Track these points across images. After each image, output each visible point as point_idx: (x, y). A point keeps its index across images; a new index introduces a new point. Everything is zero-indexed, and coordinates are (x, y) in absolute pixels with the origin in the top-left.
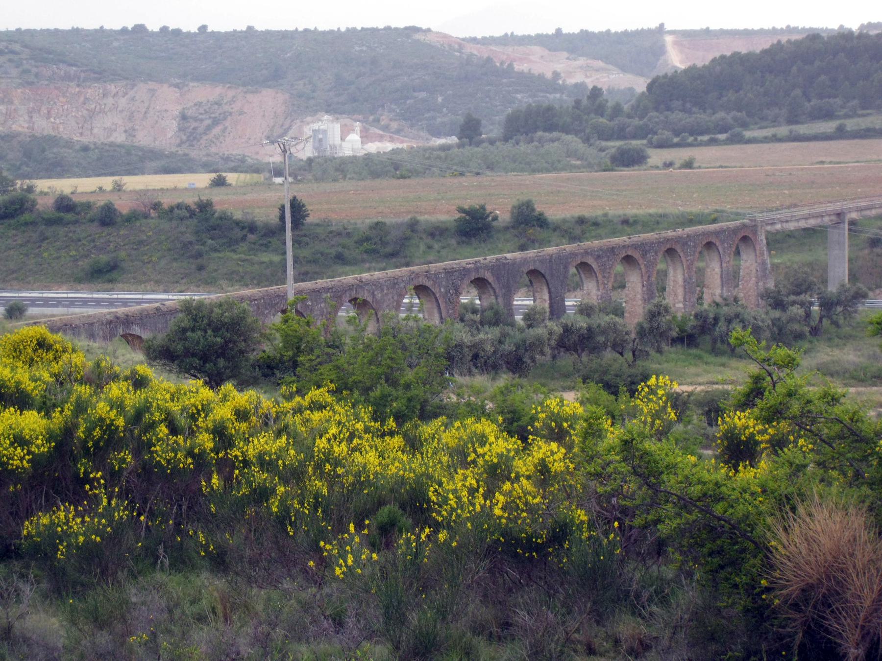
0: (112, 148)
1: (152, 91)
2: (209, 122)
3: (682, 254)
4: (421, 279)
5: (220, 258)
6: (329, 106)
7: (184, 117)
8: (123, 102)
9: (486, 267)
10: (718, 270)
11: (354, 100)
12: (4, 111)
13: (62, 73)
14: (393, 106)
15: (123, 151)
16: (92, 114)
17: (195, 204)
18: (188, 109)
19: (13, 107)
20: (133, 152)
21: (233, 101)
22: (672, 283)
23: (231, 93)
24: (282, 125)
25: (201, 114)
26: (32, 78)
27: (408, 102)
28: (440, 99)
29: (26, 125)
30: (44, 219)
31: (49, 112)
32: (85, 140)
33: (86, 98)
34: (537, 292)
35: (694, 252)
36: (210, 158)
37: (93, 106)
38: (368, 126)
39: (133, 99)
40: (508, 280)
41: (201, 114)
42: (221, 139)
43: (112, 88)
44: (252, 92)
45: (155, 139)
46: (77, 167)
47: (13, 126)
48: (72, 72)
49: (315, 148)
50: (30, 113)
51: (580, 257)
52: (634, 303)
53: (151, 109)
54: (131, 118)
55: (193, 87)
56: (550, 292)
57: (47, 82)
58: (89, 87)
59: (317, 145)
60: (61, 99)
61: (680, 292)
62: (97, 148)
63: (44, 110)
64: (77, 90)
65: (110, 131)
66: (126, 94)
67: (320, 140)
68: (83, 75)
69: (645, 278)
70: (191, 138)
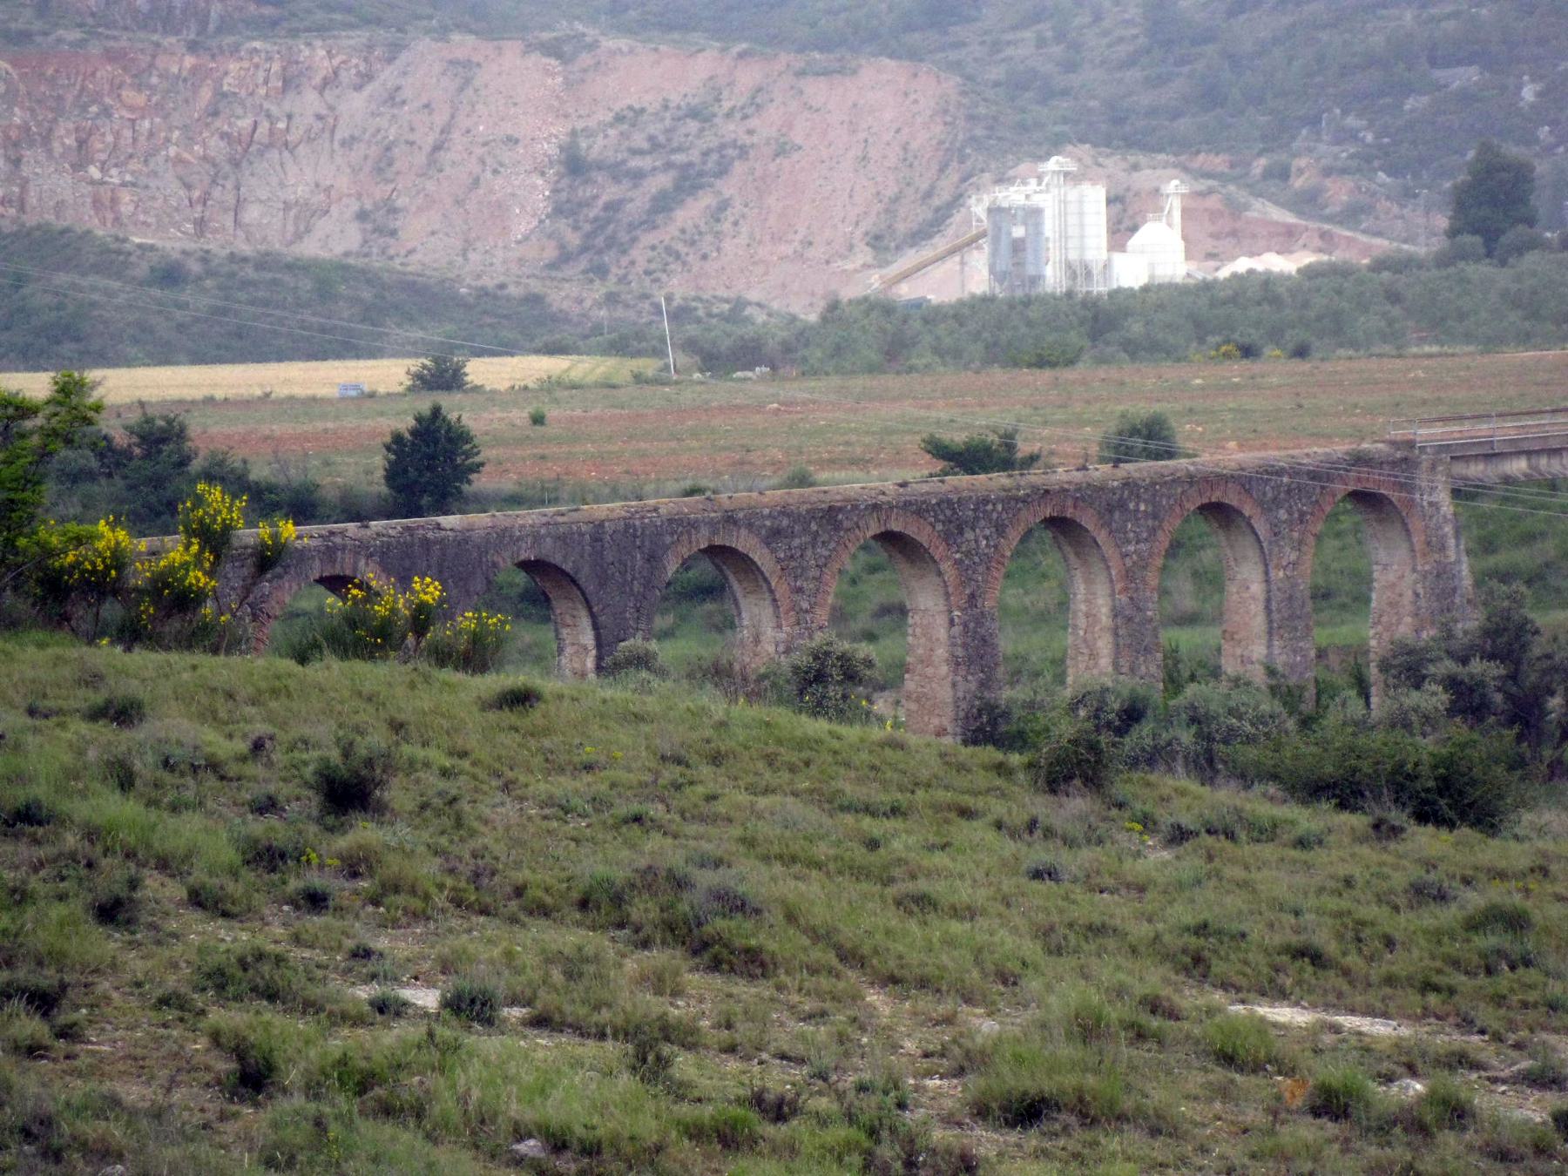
0: (269, 276)
1: (463, 70)
2: (664, 181)
3: (1102, 537)
6: (1118, 121)
7: (574, 165)
8: (355, 106)
10: (1257, 588)
11: (1211, 97)
14: (1351, 121)
15: (306, 284)
16: (243, 151)
18: (589, 133)
21: (756, 102)
23: (748, 76)
24: (929, 194)
25: (635, 152)
27: (1409, 104)
28: (1528, 93)
31: (81, 143)
33: (221, 95)
35: (1153, 531)
36: (620, 312)
37: (245, 123)
38: (1242, 196)
39: (393, 98)
41: (635, 152)
42: (707, 244)
43: (317, 56)
45: (467, 246)
46: (135, 341)
49: (997, 275)
51: (705, 531)
52: (930, 671)
53: (456, 135)
54: (383, 165)
55: (613, 53)
56: (596, 627)
57: (75, 35)
58: (234, 50)
59: (1004, 264)
60: (128, 95)
61: (1104, 645)
62: (210, 273)
64: (189, 61)
65: (305, 215)
66: (367, 77)
67: (1018, 247)
69: (959, 600)
70: (599, 241)
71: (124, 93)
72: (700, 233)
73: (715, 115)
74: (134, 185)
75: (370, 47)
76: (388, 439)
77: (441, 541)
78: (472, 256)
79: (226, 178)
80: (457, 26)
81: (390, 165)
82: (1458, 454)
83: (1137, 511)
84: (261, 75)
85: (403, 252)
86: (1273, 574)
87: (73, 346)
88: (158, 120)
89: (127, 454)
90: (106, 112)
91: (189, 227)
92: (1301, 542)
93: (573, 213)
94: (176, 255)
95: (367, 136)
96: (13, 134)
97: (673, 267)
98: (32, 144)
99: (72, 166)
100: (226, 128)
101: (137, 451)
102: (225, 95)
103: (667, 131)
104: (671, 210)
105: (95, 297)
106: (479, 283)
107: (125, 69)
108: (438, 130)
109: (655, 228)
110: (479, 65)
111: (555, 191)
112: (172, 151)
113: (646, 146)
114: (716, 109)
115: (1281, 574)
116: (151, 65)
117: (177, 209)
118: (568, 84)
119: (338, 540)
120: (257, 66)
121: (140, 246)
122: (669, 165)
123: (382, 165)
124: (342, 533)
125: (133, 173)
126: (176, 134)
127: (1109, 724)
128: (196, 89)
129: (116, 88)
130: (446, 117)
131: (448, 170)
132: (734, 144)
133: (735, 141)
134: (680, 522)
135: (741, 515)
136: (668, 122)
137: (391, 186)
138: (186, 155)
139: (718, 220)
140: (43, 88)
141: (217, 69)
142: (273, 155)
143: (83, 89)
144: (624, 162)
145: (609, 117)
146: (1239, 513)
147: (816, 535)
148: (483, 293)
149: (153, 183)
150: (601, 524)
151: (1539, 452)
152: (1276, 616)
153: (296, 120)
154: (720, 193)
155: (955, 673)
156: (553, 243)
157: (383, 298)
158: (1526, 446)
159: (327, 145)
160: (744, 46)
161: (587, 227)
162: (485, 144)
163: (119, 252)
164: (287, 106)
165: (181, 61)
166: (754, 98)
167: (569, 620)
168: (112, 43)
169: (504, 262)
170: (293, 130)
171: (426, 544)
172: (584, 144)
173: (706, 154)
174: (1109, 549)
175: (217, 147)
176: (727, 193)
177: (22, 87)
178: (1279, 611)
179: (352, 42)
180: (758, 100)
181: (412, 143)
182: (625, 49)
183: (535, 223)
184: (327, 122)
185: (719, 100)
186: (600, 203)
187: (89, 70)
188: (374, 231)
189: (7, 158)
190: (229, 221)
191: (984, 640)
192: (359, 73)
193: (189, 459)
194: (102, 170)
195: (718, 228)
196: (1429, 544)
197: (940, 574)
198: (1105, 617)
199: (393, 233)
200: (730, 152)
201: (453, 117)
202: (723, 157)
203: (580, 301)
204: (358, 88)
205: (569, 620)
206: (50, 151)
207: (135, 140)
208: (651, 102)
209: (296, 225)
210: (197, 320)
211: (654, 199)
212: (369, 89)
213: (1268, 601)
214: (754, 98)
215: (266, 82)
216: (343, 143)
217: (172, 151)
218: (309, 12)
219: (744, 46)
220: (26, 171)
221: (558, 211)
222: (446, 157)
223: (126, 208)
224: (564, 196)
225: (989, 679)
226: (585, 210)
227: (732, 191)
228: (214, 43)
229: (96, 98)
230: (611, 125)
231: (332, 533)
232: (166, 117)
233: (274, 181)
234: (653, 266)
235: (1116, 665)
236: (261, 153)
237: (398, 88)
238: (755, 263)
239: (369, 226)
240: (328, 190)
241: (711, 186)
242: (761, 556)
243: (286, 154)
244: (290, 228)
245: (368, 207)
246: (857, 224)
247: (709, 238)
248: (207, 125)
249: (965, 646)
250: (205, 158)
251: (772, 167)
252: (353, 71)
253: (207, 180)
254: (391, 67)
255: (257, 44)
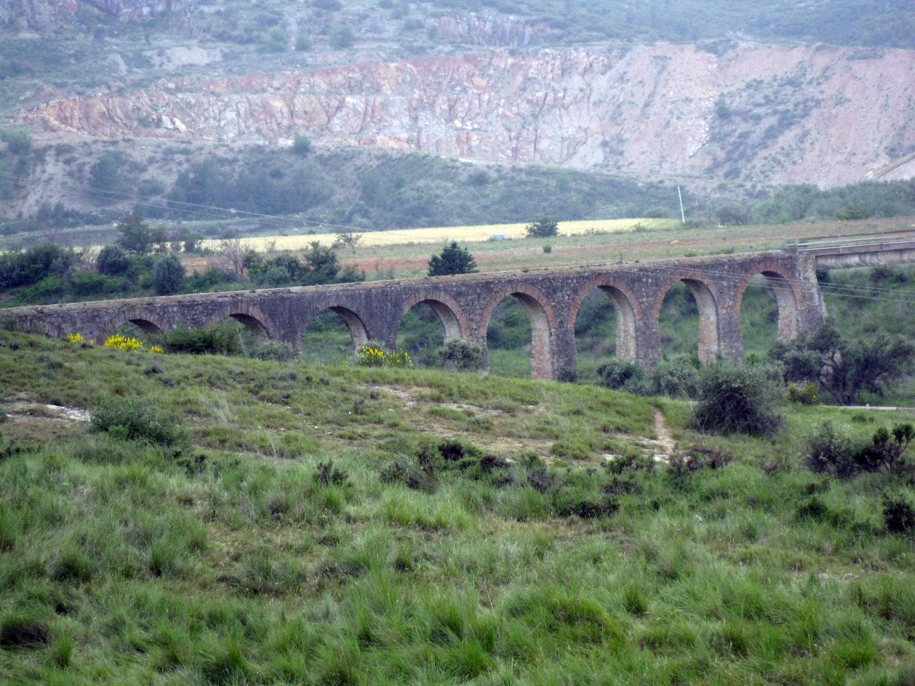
0: (533, 178)
1: (662, 62)
2: (773, 120)
3: (628, 294)
4: (137, 312)
5: (317, 340)
7: (723, 113)
8: (601, 83)
9: (251, 302)
10: (713, 318)
12: (361, 108)
13: (488, 27)
15: (553, 183)
16: (539, 109)
17: (308, 258)
18: (731, 95)
19: (379, 99)
20: (573, 185)
22: (622, 334)
23: (822, 60)
26: (421, 40)
29: (404, 135)
30: (73, 284)
31: (451, 108)
32: (479, 162)
33: (527, 79)
34: (356, 336)
35: (655, 293)
36: (727, 195)
37: (540, 94)
40: (290, 318)
42: (796, 156)
43: (580, 55)
44: (865, 58)
46: (460, 216)
47: (378, 138)
48: (508, 26)
50: (414, 112)
52: (542, 357)
53: (657, 98)
54: (616, 116)
57: (449, 48)
58: (535, 55)
60: (477, 80)
61: (632, 345)
63: (442, 104)
64: (511, 61)
65: (573, 145)
66: (609, 67)
68: (529, 30)
71: (474, 79)
72: (792, 150)
73: (802, 83)
74: (479, 130)
75: (610, 50)
76: (430, 260)
77: (290, 298)
78: (665, 165)
79: (530, 125)
80: (662, 37)
81: (620, 115)
82: (819, 255)
83: (647, 282)
84: (549, 68)
85: (627, 163)
86: (720, 311)
87: (426, 219)
88: (492, 94)
89: (306, 270)
90: (465, 90)
91: (509, 152)
92: (735, 296)
93: (722, 139)
94: (484, 169)
95: (607, 100)
96: (414, 104)
97: (776, 169)
98: (424, 109)
99: (446, 120)
100: (530, 97)
101: (312, 268)
102: (529, 79)
103: (776, 93)
104: (776, 137)
105: (438, 192)
106: (649, 180)
107: (476, 66)
108: (647, 95)
109: (768, 147)
110: (670, 59)
111: (712, 128)
112: (500, 110)
113: (763, 101)
114: (802, 79)
115: (724, 311)
116: (490, 64)
117: (502, 143)
118: (720, 68)
119: (239, 298)
120: (547, 63)
121: (464, 164)
122: (775, 112)
123: (616, 116)
124: (242, 295)
125: (478, 123)
126: (503, 101)
127: (614, 379)
128: (514, 76)
129: (470, 76)
130: (651, 88)
131: (652, 118)
132: (812, 99)
133: (813, 98)
134: (410, 289)
135: (441, 285)
136: (776, 88)
137: (620, 128)
138: (508, 113)
139: (802, 142)
140: (431, 78)
141: (526, 65)
142: (556, 111)
143: (451, 79)
144: (750, 111)
145: (743, 86)
146: (701, 283)
147: (479, 295)
148: (651, 186)
149: (490, 128)
150: (370, 290)
151: (865, 253)
152: (722, 331)
153: (569, 92)
154: (804, 127)
155: (553, 357)
156: (711, 157)
157: (595, 189)
158: (856, 250)
159: (586, 105)
160: (820, 44)
161: (730, 148)
162: (673, 103)
163: (453, 168)
164: (564, 84)
165: (506, 61)
166: (824, 72)
167: (357, 333)
168: (469, 52)
169: (683, 168)
170: (567, 98)
171: (283, 299)
172: (728, 101)
173: (797, 105)
174: (633, 301)
175: (525, 108)
176: (808, 126)
177: (418, 77)
178: (723, 329)
179: (600, 48)
180: (827, 74)
181: (633, 103)
182: (753, 47)
183: (700, 145)
184: (585, 93)
185: (805, 75)
186: (737, 134)
187: (456, 67)
188: (611, 152)
189: (411, 117)
190: (531, 149)
191: (567, 342)
192: (604, 65)
193: (336, 271)
194: (462, 122)
195: (802, 146)
196: (804, 297)
197: (544, 312)
198: (632, 330)
199: (621, 153)
200: (810, 104)
201: (655, 87)
202: (806, 106)
203: (705, 189)
204: (603, 73)
205: (357, 333)
206: (433, 112)
207: (480, 105)
208: (767, 77)
209: (568, 149)
210: (493, 203)
211: (767, 131)
212: (609, 73)
213: (718, 324)
214: (824, 72)
215: (552, 71)
216: (595, 104)
217: (500, 110)
218: (580, 31)
219: (820, 44)
220: (421, 124)
221: (713, 139)
222: (651, 110)
223: (475, 142)
224: (716, 130)
225: (570, 360)
226: (728, 139)
227: (811, 125)
228: (524, 50)
229: (459, 83)
230: (744, 90)
231: (237, 295)
232: (497, 92)
233: (556, 126)
234: (765, 169)
235: (638, 356)
236: (549, 111)
237: (625, 73)
238: (822, 166)
239: (608, 150)
240: (586, 130)
241: (799, 123)
242: (451, 304)
243: (563, 110)
244: (565, 152)
245: (608, 139)
246: (881, 142)
247: (797, 152)
248: (520, 96)
249: (558, 345)
250: (518, 114)
251: (834, 112)
252: (601, 64)
253: (519, 126)
254: (622, 61)
255: (547, 50)
